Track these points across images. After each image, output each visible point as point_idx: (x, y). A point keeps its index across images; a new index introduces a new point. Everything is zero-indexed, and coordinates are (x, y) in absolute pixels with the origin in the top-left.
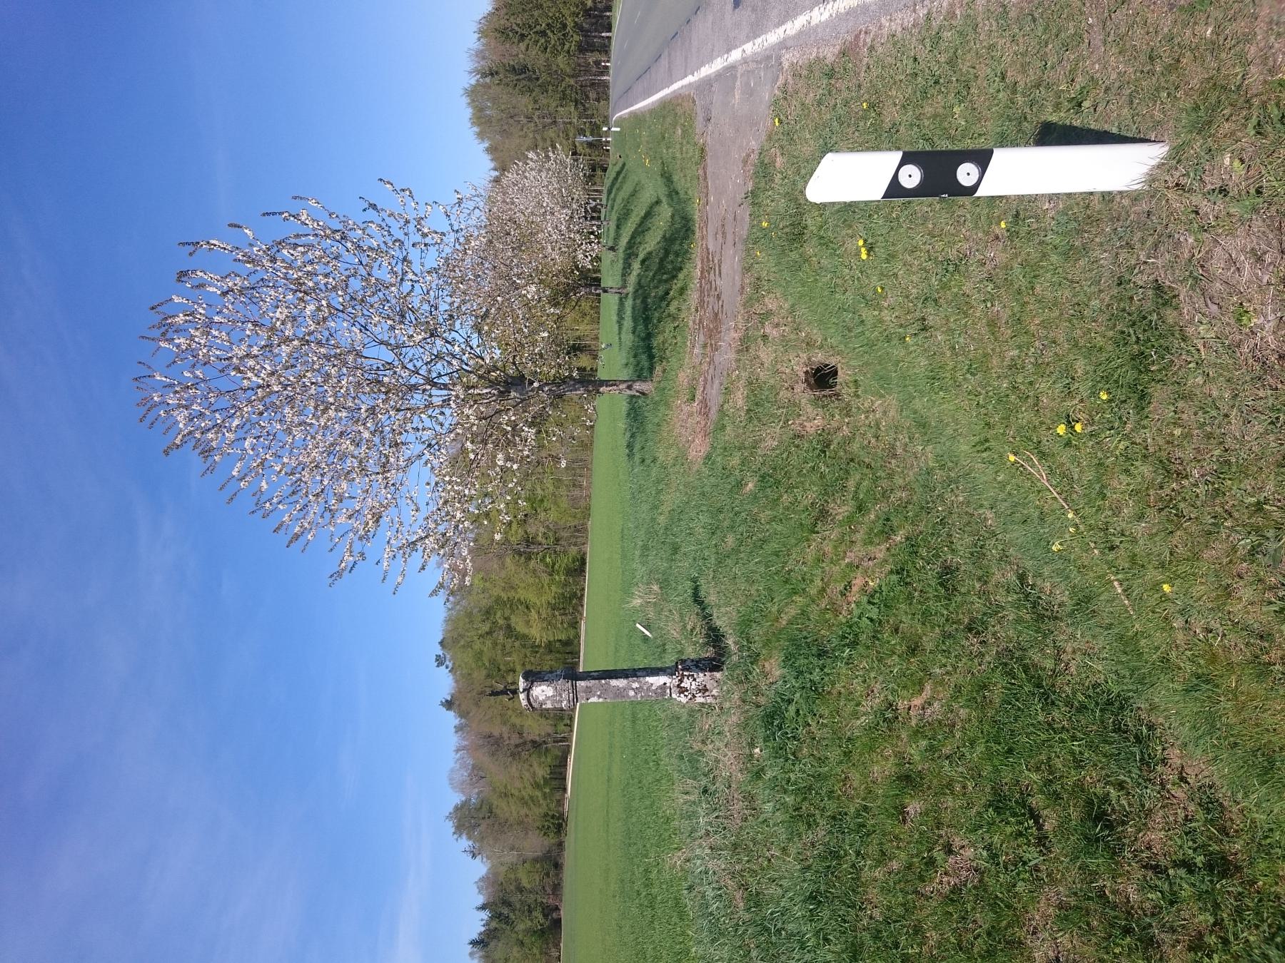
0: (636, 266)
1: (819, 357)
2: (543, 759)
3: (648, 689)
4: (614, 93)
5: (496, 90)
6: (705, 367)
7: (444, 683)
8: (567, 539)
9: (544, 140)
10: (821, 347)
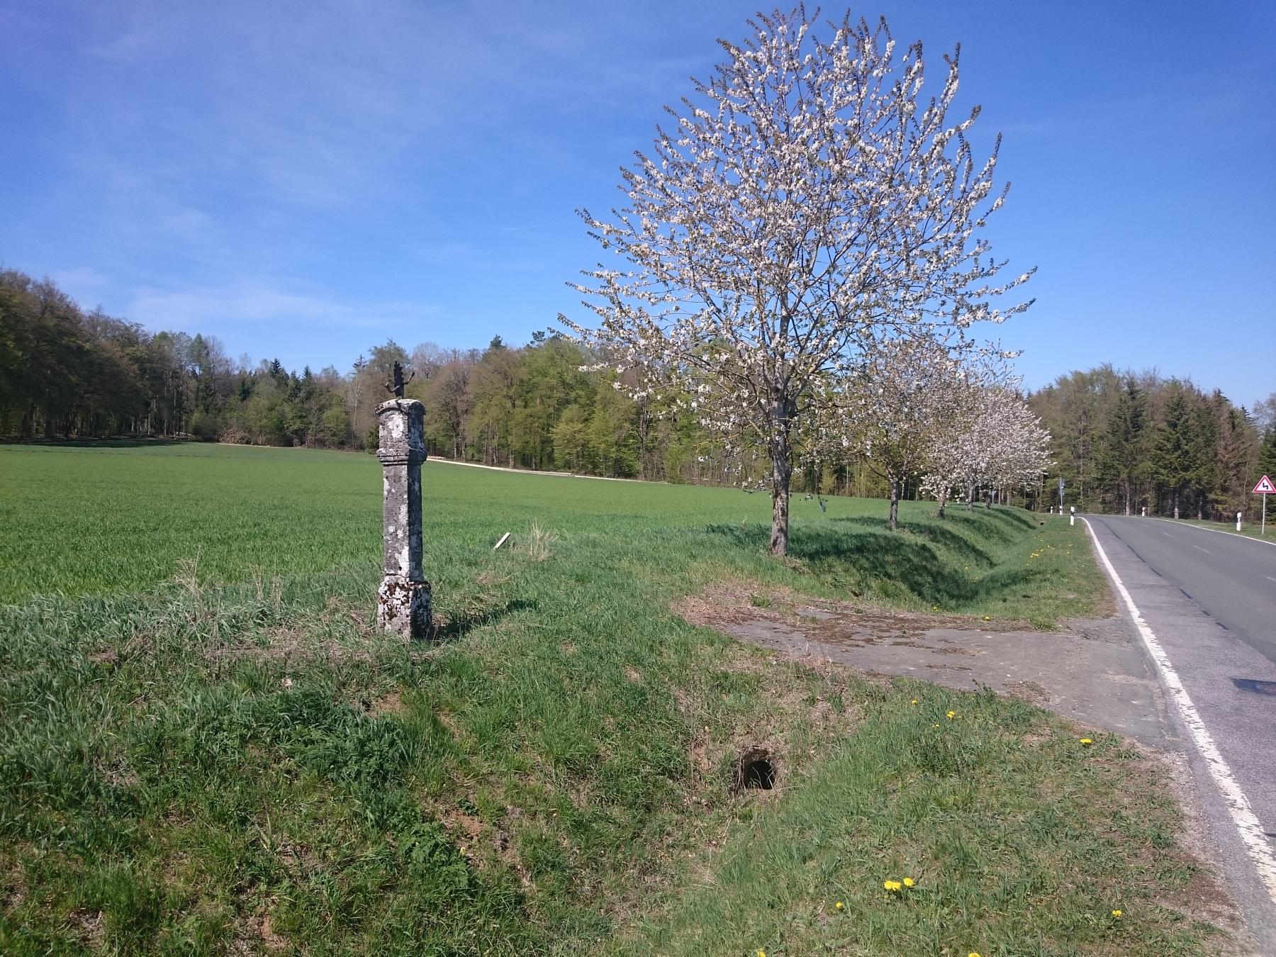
0: (921, 540)
1: (783, 770)
2: (442, 433)
3: (396, 549)
4: (1111, 519)
5: (1115, 399)
6: (790, 620)
7: (517, 340)
8: (651, 461)
9: (1060, 446)
10: (795, 774)
